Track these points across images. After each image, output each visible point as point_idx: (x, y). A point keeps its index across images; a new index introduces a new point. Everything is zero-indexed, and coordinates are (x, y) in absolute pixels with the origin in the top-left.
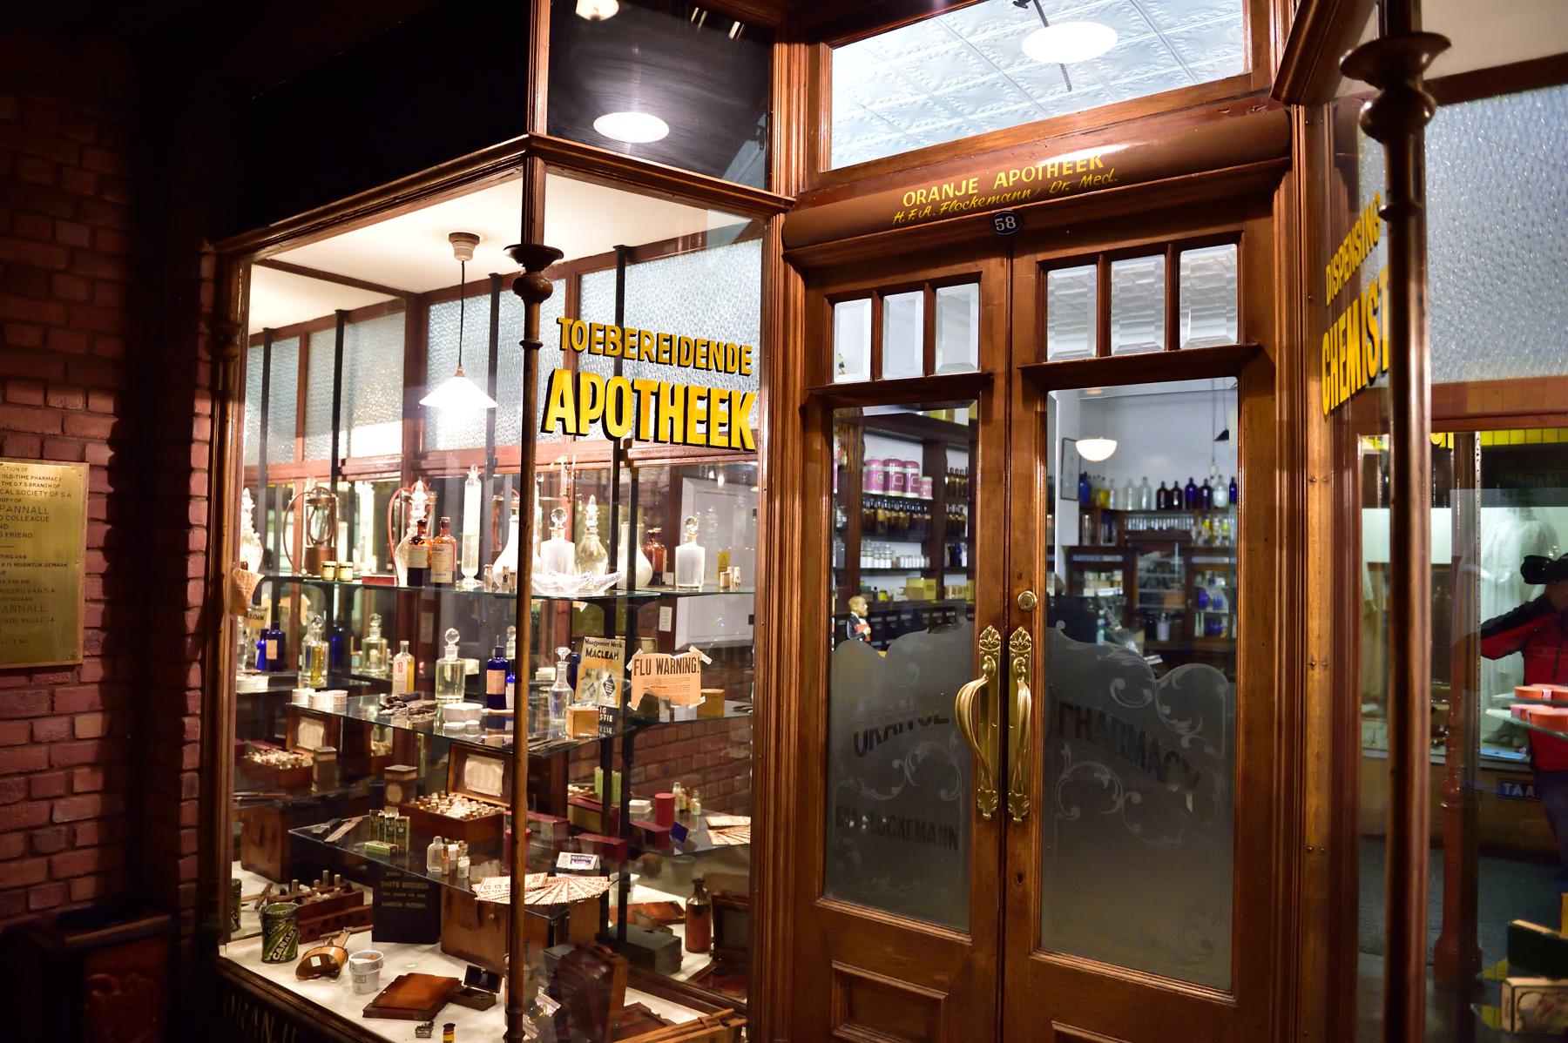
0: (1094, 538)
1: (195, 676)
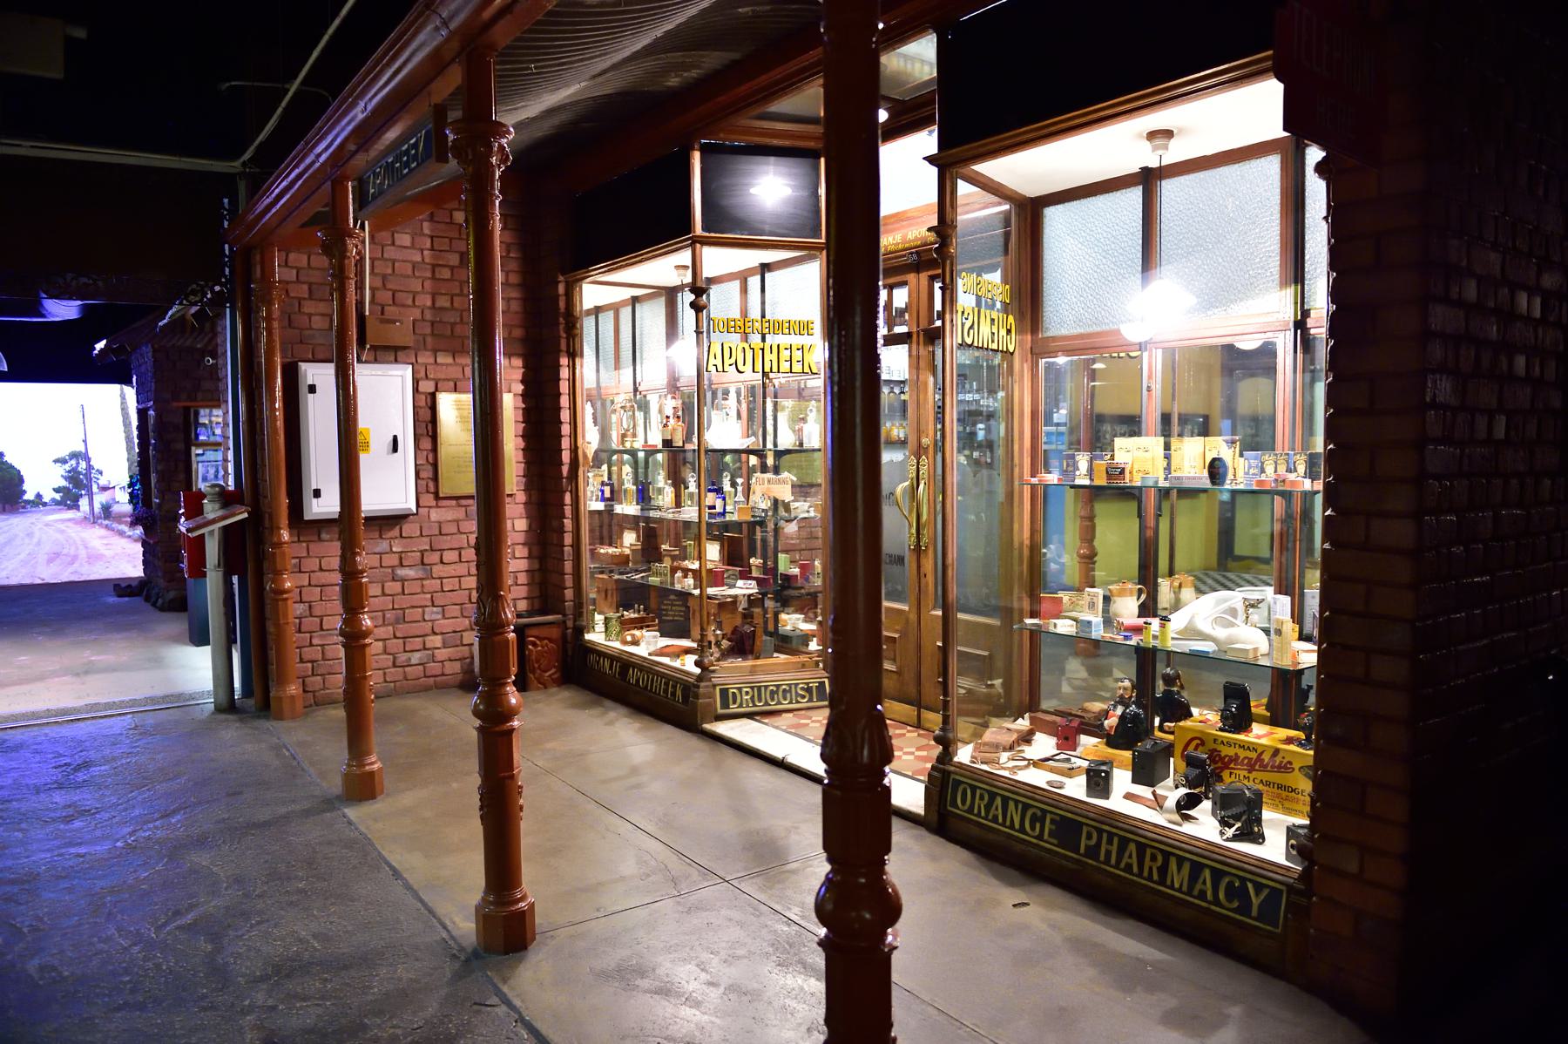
1: (568, 498)
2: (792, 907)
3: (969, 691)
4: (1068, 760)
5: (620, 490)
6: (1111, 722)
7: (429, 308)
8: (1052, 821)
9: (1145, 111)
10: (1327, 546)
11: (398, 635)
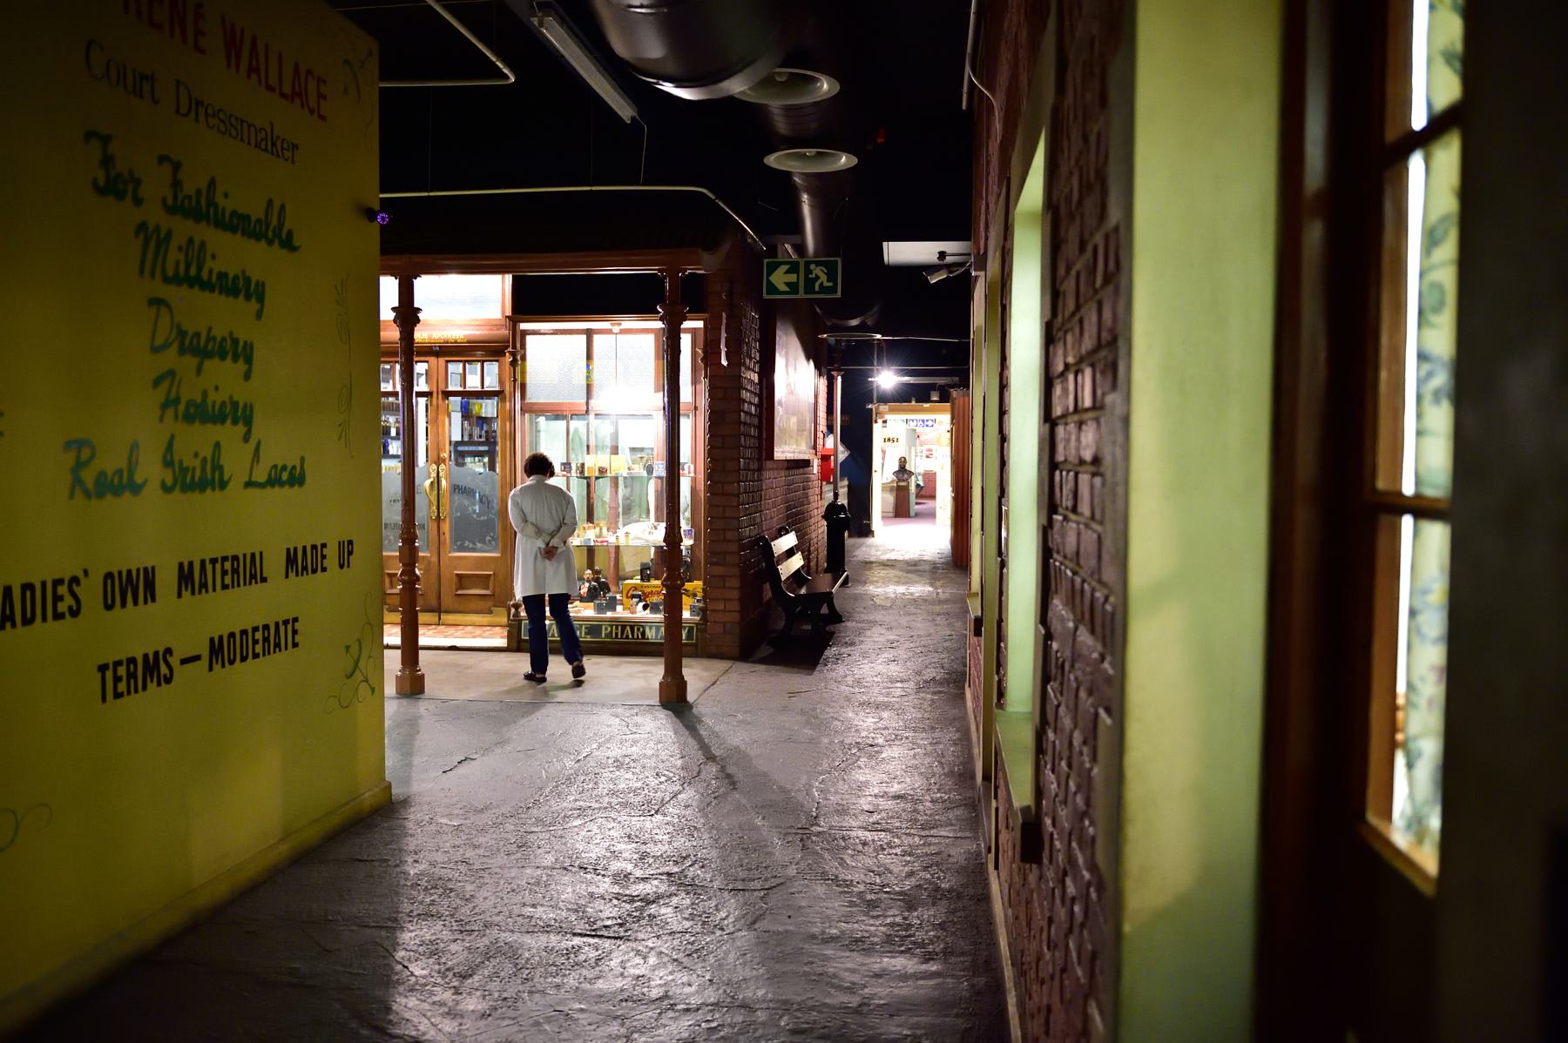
0: (471, 436)
8: (586, 628)
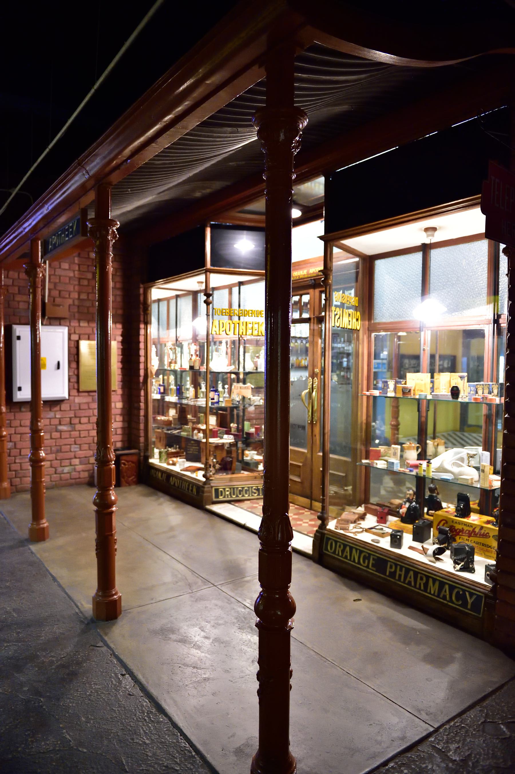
1: (142, 393)
2: (246, 599)
3: (336, 493)
4: (382, 529)
5: (168, 389)
6: (403, 511)
7: (77, 299)
8: (373, 559)
9: (423, 219)
10: (505, 432)
11: (58, 458)
